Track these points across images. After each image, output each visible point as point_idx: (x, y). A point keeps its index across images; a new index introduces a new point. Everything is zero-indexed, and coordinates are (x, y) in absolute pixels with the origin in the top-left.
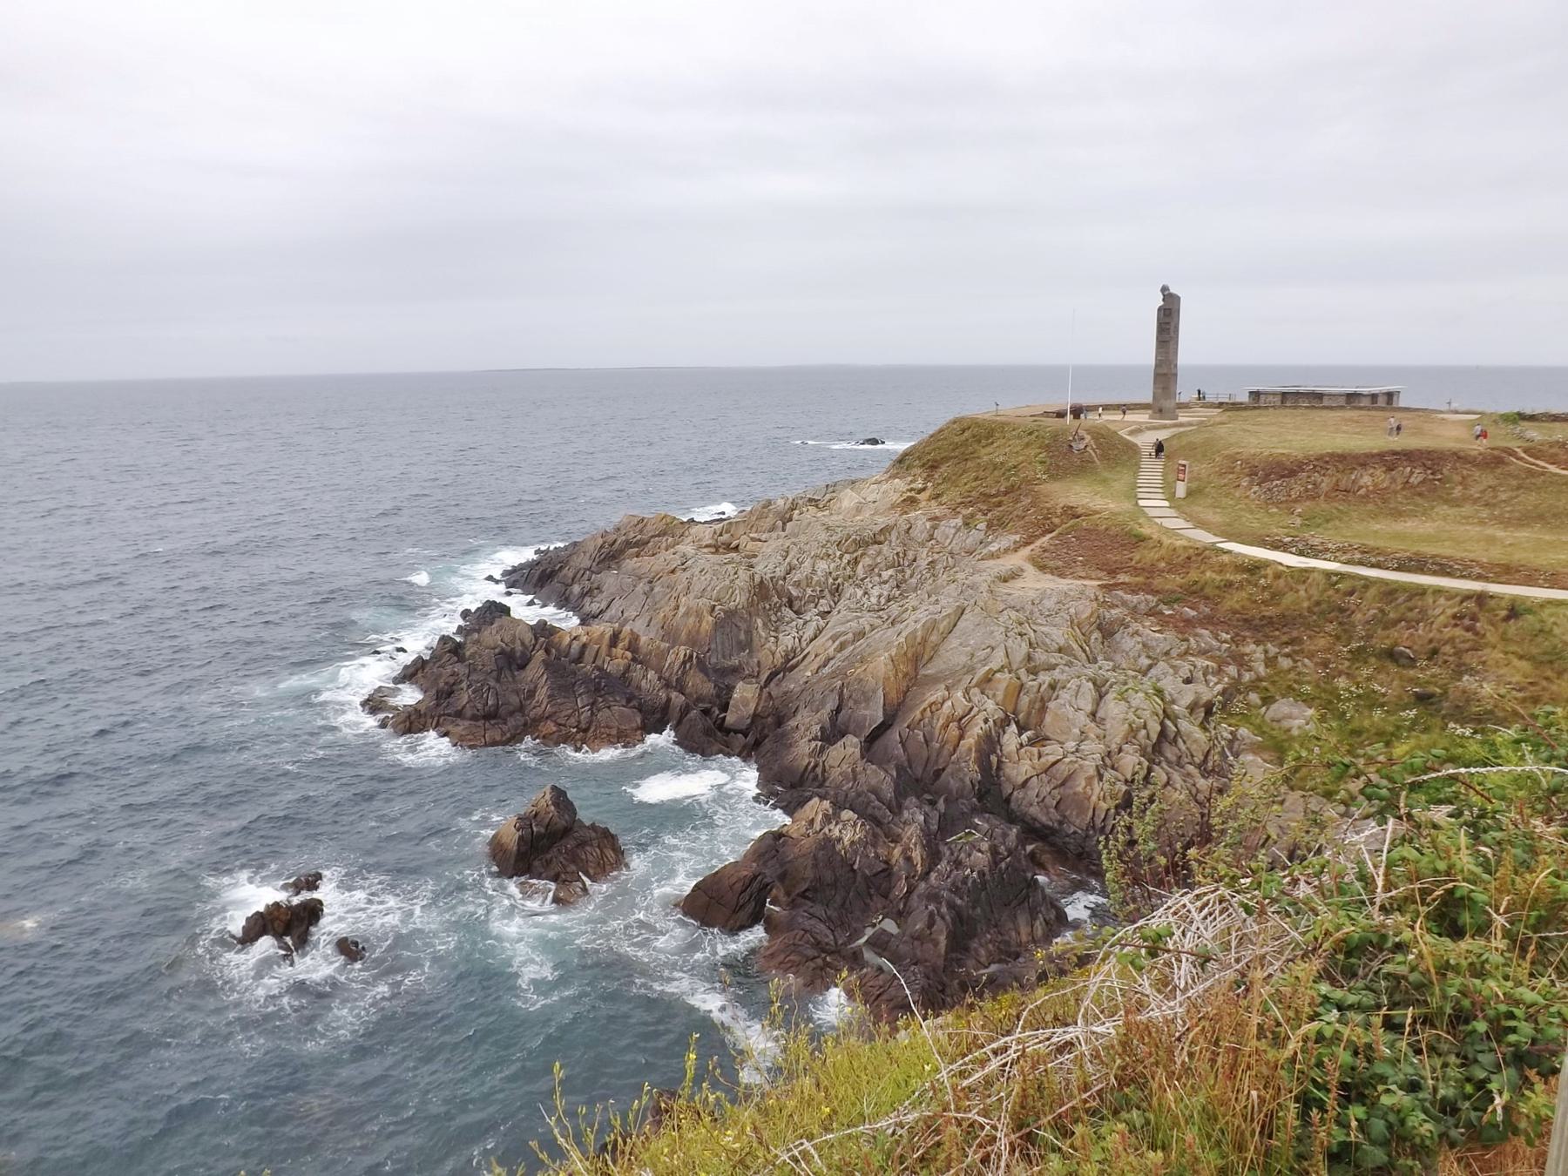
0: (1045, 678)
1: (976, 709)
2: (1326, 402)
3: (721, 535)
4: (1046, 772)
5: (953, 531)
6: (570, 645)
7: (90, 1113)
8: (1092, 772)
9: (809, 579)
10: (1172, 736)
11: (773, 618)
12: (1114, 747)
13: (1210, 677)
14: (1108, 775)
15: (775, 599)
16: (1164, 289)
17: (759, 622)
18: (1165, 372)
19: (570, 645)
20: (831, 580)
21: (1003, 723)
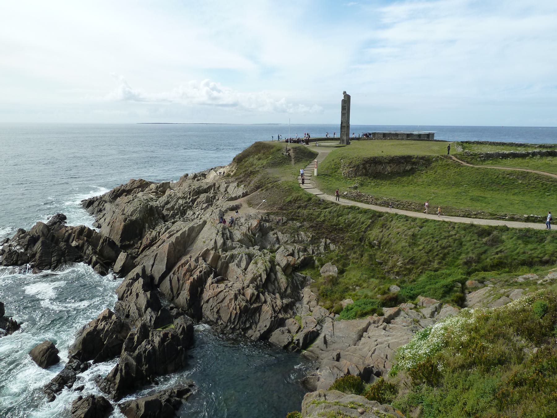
0: (229, 254)
1: (199, 266)
2: (400, 138)
3: (160, 188)
4: (217, 296)
5: (234, 188)
6: (65, 234)
7: (325, 337)
8: (232, 296)
9: (173, 208)
10: (273, 280)
11: (154, 224)
12: (246, 285)
13: (300, 253)
14: (240, 297)
15: (156, 216)
16: (345, 93)
17: (147, 225)
18: (345, 125)
19: (65, 234)
20: (182, 208)
21: (207, 274)
